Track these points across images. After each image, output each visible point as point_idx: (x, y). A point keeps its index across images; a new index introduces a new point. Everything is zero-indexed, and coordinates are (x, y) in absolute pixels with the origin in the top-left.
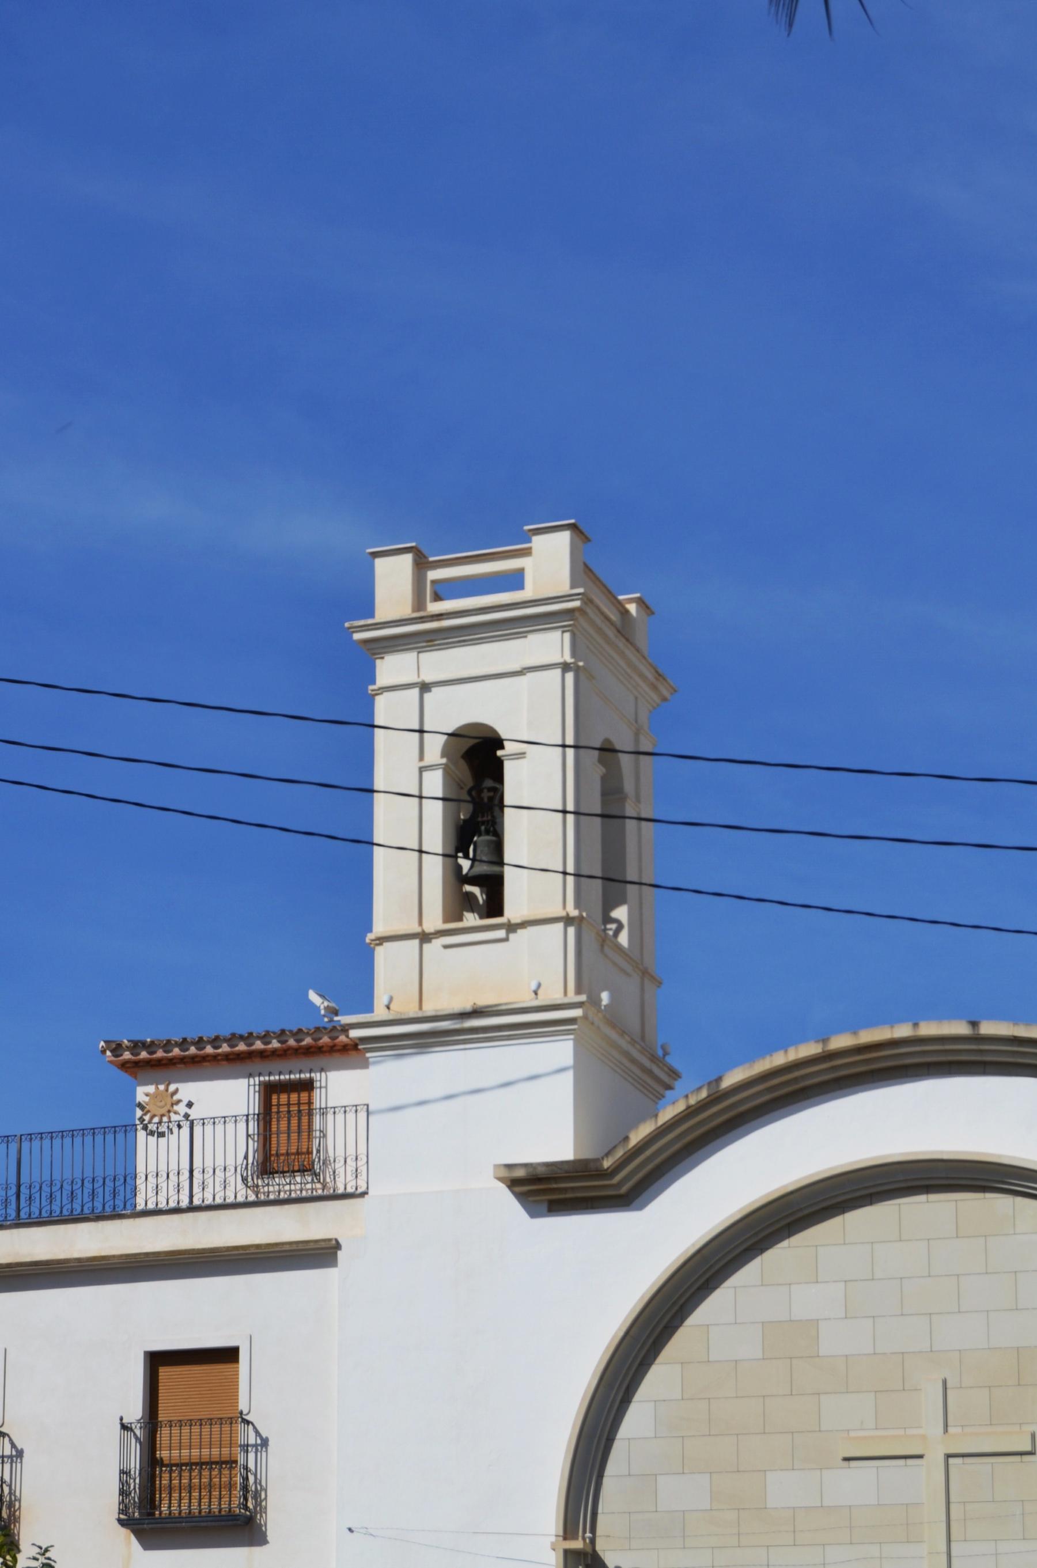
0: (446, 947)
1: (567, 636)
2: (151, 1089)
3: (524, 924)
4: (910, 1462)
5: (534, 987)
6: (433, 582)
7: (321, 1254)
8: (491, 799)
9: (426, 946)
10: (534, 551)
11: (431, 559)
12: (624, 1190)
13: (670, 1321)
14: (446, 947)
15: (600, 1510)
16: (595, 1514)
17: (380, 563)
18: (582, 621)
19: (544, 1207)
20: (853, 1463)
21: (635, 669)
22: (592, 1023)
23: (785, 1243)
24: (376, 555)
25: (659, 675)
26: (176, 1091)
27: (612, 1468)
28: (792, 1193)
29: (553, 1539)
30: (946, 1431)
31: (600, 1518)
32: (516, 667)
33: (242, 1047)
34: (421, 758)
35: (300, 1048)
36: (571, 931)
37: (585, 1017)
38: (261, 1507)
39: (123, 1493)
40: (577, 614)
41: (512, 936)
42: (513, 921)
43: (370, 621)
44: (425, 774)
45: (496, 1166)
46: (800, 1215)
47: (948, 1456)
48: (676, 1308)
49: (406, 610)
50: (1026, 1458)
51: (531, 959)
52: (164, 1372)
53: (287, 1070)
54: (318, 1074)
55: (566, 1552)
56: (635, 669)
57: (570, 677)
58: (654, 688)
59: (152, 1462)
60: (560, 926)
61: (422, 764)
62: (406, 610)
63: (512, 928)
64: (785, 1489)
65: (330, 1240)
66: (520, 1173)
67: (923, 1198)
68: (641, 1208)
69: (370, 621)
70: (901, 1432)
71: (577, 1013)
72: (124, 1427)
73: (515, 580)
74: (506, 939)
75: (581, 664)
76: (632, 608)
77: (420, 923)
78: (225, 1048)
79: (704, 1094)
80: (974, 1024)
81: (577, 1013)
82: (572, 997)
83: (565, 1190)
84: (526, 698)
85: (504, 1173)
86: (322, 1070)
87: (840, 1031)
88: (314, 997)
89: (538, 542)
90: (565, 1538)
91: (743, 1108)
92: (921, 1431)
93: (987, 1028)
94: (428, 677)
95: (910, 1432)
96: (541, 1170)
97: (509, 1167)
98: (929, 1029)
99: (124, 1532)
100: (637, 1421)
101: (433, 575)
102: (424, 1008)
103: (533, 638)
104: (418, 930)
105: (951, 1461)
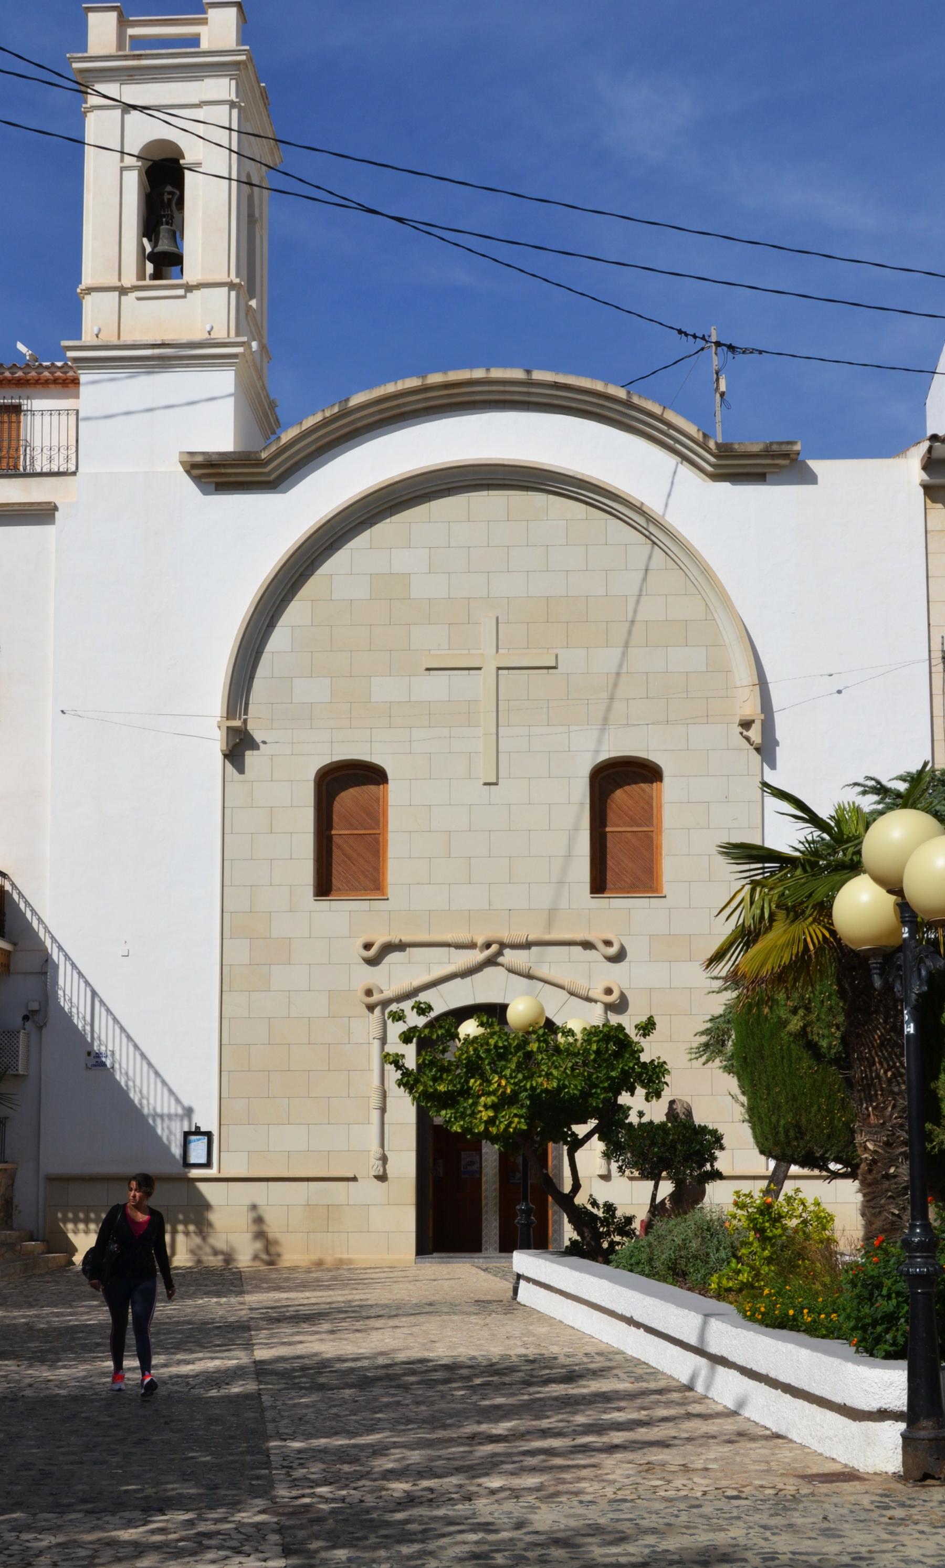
0: (139, 299)
1: (233, 83)
3: (198, 286)
4: (471, 672)
6: (130, 36)
7: (42, 514)
8: (170, 200)
9: (123, 298)
11: (131, 18)
12: (272, 477)
13: (304, 570)
14: (139, 299)
15: (251, 702)
16: (247, 704)
17: (92, 16)
23: (388, 520)
28: (397, 483)
29: (219, 719)
30: (497, 652)
31: (251, 707)
35: (13, 379)
36: (233, 294)
41: (188, 294)
42: (190, 283)
43: (86, 55)
44: (124, 173)
45: (180, 453)
47: (499, 668)
49: (112, 49)
50: (551, 671)
51: (203, 310)
54: (25, 402)
55: (228, 728)
60: (226, 289)
61: (122, 165)
62: (112, 49)
63: (189, 288)
64: (385, 689)
65: (50, 503)
66: (199, 459)
67: (485, 493)
68: (285, 491)
69: (80, 55)
70: (467, 652)
71: (239, 350)
73: (195, 40)
74: (184, 297)
75: (243, 104)
77: (120, 280)
79: (336, 409)
80: (528, 372)
81: (239, 350)
82: (233, 338)
83: (230, 475)
84: (204, 122)
85: (186, 458)
86: (28, 398)
88: (21, 347)
89: (212, 13)
91: (359, 424)
93: (538, 375)
95: (472, 652)
96: (214, 457)
97: (191, 454)
98: (497, 373)
100: (279, 640)
101: (131, 31)
102: (122, 339)
103: (207, 81)
104: (119, 284)
105: (501, 672)
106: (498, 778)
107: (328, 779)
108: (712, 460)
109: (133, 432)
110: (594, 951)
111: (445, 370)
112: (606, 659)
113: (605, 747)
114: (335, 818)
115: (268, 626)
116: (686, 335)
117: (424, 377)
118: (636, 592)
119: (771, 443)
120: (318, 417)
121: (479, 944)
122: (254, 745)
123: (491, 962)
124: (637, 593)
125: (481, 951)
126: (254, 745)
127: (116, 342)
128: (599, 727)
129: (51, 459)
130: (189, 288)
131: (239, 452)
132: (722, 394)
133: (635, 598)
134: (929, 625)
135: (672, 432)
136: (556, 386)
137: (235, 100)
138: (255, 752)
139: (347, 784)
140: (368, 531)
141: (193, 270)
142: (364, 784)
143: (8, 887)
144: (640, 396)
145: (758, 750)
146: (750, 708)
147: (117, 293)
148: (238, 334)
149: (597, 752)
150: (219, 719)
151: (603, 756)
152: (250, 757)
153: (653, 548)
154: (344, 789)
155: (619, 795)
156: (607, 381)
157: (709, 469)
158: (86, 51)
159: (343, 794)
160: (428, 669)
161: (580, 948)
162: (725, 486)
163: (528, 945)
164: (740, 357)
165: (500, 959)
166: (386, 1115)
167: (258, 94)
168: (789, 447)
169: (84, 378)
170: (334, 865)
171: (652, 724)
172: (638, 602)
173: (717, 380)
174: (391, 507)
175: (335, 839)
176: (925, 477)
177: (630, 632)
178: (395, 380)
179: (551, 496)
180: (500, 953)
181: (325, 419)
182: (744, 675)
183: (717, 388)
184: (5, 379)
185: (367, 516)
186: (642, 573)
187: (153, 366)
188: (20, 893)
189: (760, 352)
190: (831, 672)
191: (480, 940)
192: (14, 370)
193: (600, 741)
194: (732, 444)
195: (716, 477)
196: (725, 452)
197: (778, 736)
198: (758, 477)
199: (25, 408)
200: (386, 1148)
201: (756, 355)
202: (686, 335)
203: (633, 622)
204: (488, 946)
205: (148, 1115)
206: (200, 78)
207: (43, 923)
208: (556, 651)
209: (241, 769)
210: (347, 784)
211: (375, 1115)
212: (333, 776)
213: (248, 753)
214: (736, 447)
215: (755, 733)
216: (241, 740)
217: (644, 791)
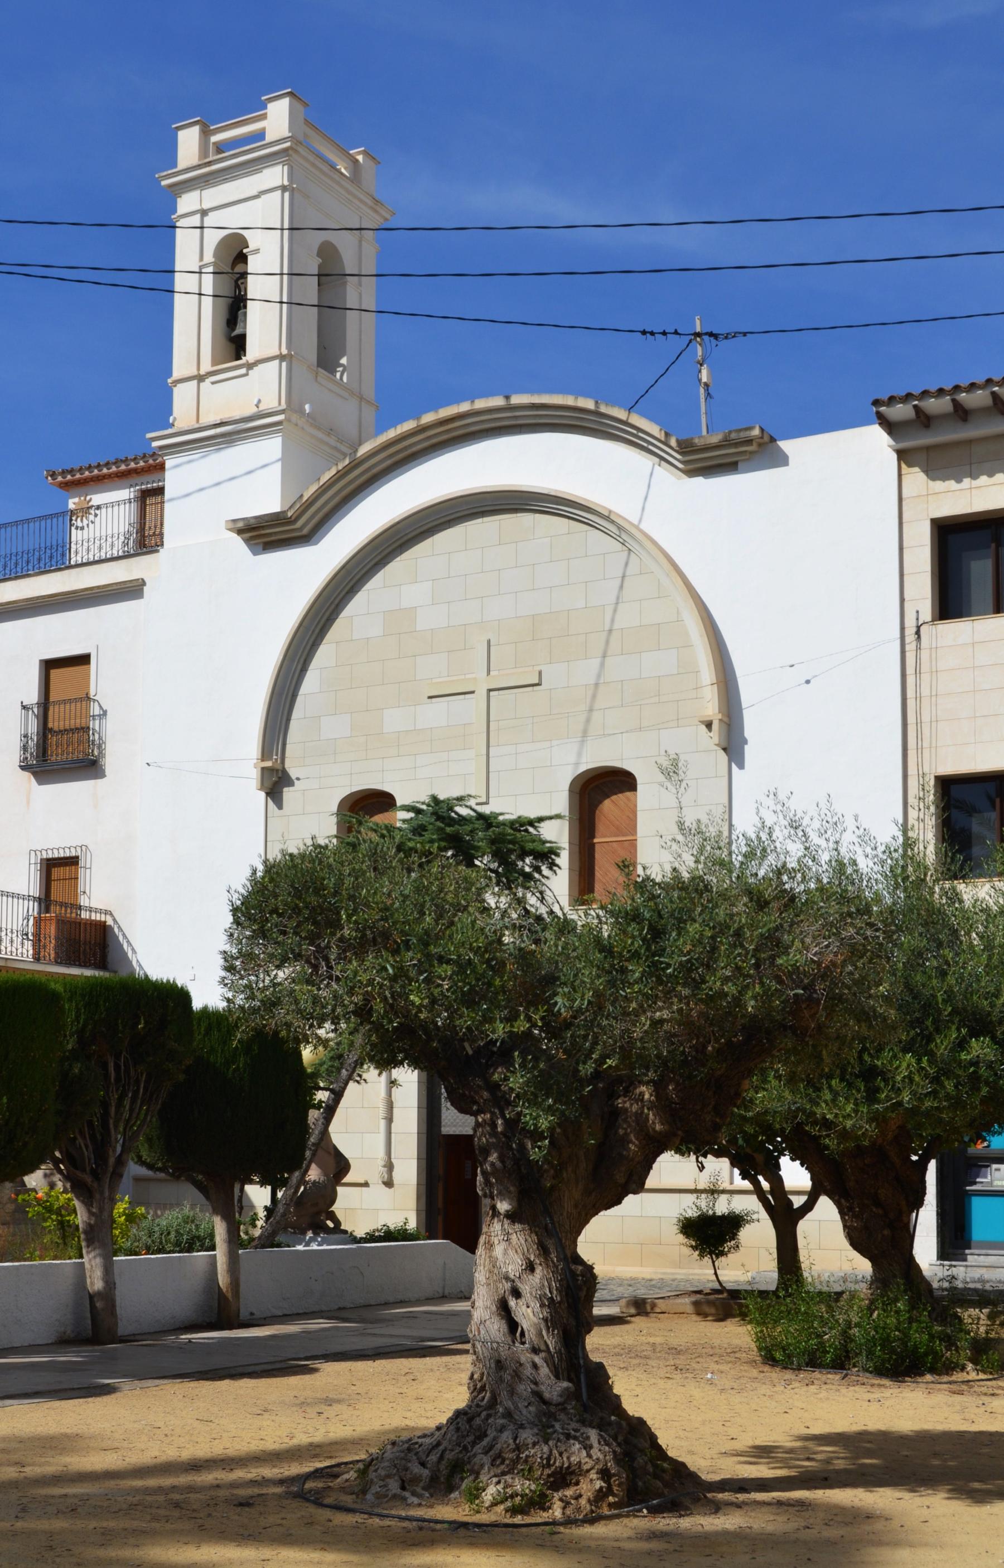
1: (286, 167)
2: (76, 500)
4: (467, 696)
5: (255, 402)
6: (214, 143)
7: (132, 590)
10: (268, 115)
12: (305, 531)
18: (295, 156)
19: (261, 547)
20: (434, 700)
21: (355, 196)
22: (296, 425)
23: (398, 559)
24: (179, 128)
25: (377, 202)
26: (91, 500)
27: (295, 715)
28: (398, 523)
30: (489, 673)
32: (255, 193)
33: (123, 467)
34: (201, 258)
37: (288, 420)
38: (102, 754)
39: (25, 748)
40: (290, 152)
41: (250, 372)
45: (227, 521)
46: (405, 538)
47: (490, 690)
48: (333, 606)
50: (536, 688)
51: (259, 386)
52: (54, 673)
53: (144, 477)
55: (263, 769)
56: (355, 196)
57: (287, 195)
58: (376, 211)
59: (45, 730)
60: (277, 362)
62: (195, 161)
63: (250, 366)
64: (394, 720)
66: (240, 525)
67: (480, 520)
68: (316, 543)
70: (463, 677)
72: (24, 707)
73: (260, 135)
74: (247, 375)
76: (360, 158)
78: (114, 469)
79: (347, 462)
80: (507, 398)
83: (271, 534)
84: (255, 208)
85: (231, 526)
87: (427, 411)
90: (263, 760)
92: (474, 676)
93: (516, 400)
94: (205, 206)
95: (467, 676)
96: (253, 521)
97: (234, 521)
98: (480, 404)
99: (27, 775)
101: (215, 139)
105: (492, 693)
106: (488, 797)
108: (679, 457)
110: (97, 895)
111: (435, 408)
112: (586, 671)
113: (584, 760)
116: (652, 333)
117: (418, 418)
118: (614, 600)
120: (333, 471)
124: (614, 601)
127: (197, 426)
128: (579, 739)
129: (100, 548)
132: (706, 385)
133: (612, 607)
135: (640, 434)
136: (534, 406)
137: (286, 183)
138: (291, 788)
140: (382, 572)
141: (253, 350)
143: (110, 922)
144: (607, 405)
145: (725, 749)
146: (711, 707)
149: (577, 764)
150: (255, 761)
151: (583, 768)
152: (288, 793)
153: (629, 554)
156: (578, 393)
160: (430, 697)
162: (699, 480)
164: (723, 344)
166: (393, 1125)
168: (747, 434)
169: (169, 463)
172: (615, 611)
176: (892, 442)
177: (607, 642)
178: (394, 425)
179: (537, 515)
181: (338, 472)
182: (707, 674)
183: (700, 380)
185: (379, 557)
186: (618, 581)
187: (219, 444)
188: (119, 927)
189: (745, 334)
190: (791, 663)
193: (579, 754)
194: (692, 439)
195: (691, 473)
197: (748, 733)
200: (393, 1156)
201: (740, 339)
202: (652, 333)
203: (610, 631)
206: (259, 171)
208: (538, 668)
209: (280, 806)
211: (383, 1124)
213: (285, 790)
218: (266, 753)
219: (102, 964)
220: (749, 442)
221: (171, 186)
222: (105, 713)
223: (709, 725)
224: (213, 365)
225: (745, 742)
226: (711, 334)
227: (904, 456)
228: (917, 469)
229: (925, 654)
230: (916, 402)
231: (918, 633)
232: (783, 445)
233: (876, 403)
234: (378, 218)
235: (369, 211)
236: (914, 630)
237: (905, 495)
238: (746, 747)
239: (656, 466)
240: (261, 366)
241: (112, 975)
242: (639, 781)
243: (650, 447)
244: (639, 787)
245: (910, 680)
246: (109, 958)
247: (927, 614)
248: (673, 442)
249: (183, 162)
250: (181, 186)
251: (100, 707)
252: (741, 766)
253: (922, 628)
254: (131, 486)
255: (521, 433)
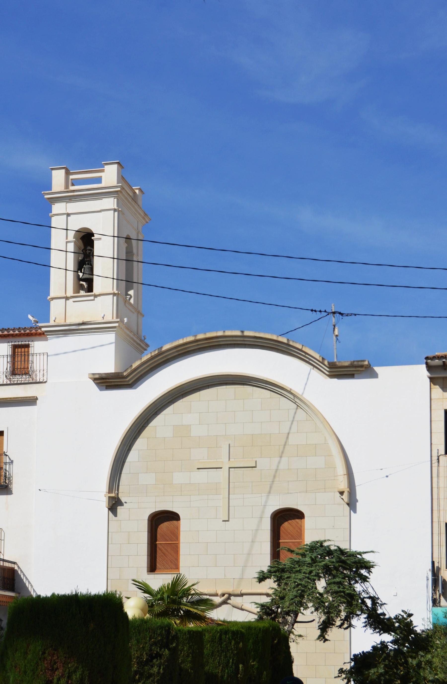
0: (74, 302)
1: (116, 200)
3: (100, 295)
4: (218, 469)
5: (102, 316)
6: (72, 179)
7: (31, 401)
10: (105, 171)
12: (130, 382)
14: (74, 302)
17: (54, 172)
18: (121, 195)
19: (105, 387)
23: (181, 400)
25: (145, 214)
28: (154, 403)
29: (105, 493)
33: (6, 333)
36: (115, 298)
37: (119, 326)
40: (119, 192)
43: (50, 192)
46: (186, 391)
47: (230, 468)
48: (146, 420)
50: (253, 468)
51: (101, 306)
55: (109, 497)
58: (144, 218)
62: (63, 189)
63: (96, 296)
64: (179, 478)
66: (97, 376)
70: (216, 460)
71: (116, 325)
73: (99, 180)
74: (94, 300)
75: (120, 209)
76: (137, 191)
77: (66, 294)
79: (157, 352)
80: (242, 332)
81: (116, 325)
82: (115, 319)
83: (112, 382)
85: (92, 376)
86: (32, 341)
88: (30, 317)
89: (106, 167)
90: (109, 493)
92: (222, 460)
93: (247, 333)
95: (218, 460)
96: (104, 376)
97: (93, 374)
98: (228, 333)
100: (133, 456)
101: (72, 177)
104: (65, 296)
106: (229, 518)
107: (156, 518)
108: (328, 369)
109: (72, 360)
114: (158, 536)
115: (128, 450)
116: (315, 311)
119: (354, 361)
121: (219, 595)
122: (121, 504)
123: (225, 602)
125: (221, 598)
126: (121, 504)
130: (96, 296)
131: (116, 373)
132: (337, 336)
134: (431, 444)
135: (307, 356)
137: (116, 208)
138: (122, 507)
139: (162, 522)
141: (97, 289)
142: (171, 520)
143: (16, 568)
145: (348, 504)
146: (343, 485)
147: (64, 300)
148: (117, 318)
150: (105, 493)
154: (162, 522)
155: (286, 525)
157: (327, 373)
158: (51, 190)
159: (162, 525)
160: (198, 469)
161: (265, 596)
162: (335, 380)
163: (242, 595)
164: (345, 318)
165: (229, 601)
167: (130, 200)
170: (157, 557)
171: (300, 492)
173: (334, 329)
174: (182, 395)
175: (158, 546)
176: (429, 375)
179: (254, 388)
180: (229, 598)
181: (152, 356)
182: (341, 470)
184: (22, 334)
185: (171, 399)
188: (21, 571)
189: (355, 315)
191: (220, 593)
192: (25, 330)
196: (332, 366)
197: (358, 497)
198: (351, 376)
199: (31, 346)
201: (353, 317)
202: (315, 311)
204: (223, 595)
205: (434, 677)
206: (101, 199)
207: (30, 583)
208: (255, 459)
209: (115, 515)
210: (162, 522)
212: (157, 517)
213: (119, 507)
214: (337, 363)
215: (345, 496)
216: (116, 502)
217: (298, 523)
218: (110, 490)
219: (12, 589)
220: (362, 366)
221: (49, 198)
222: (12, 462)
223: (342, 493)
224: (74, 293)
225: (357, 501)
226: (340, 313)
227: (432, 380)
228: (437, 387)
229: (441, 469)
230: (444, 360)
231: (438, 459)
232: (376, 369)
233: (427, 358)
234: (144, 221)
235: (141, 219)
236: (437, 458)
237: (432, 398)
238: (357, 503)
239: (312, 370)
240: (102, 297)
241: (18, 595)
242: (305, 516)
243: (311, 362)
244: (305, 518)
245: (435, 480)
246: (16, 587)
247: (442, 451)
248: (326, 363)
249: (55, 188)
250: (55, 199)
251: (10, 459)
252: (355, 512)
253: (440, 457)
254: (8, 342)
255: (245, 347)
